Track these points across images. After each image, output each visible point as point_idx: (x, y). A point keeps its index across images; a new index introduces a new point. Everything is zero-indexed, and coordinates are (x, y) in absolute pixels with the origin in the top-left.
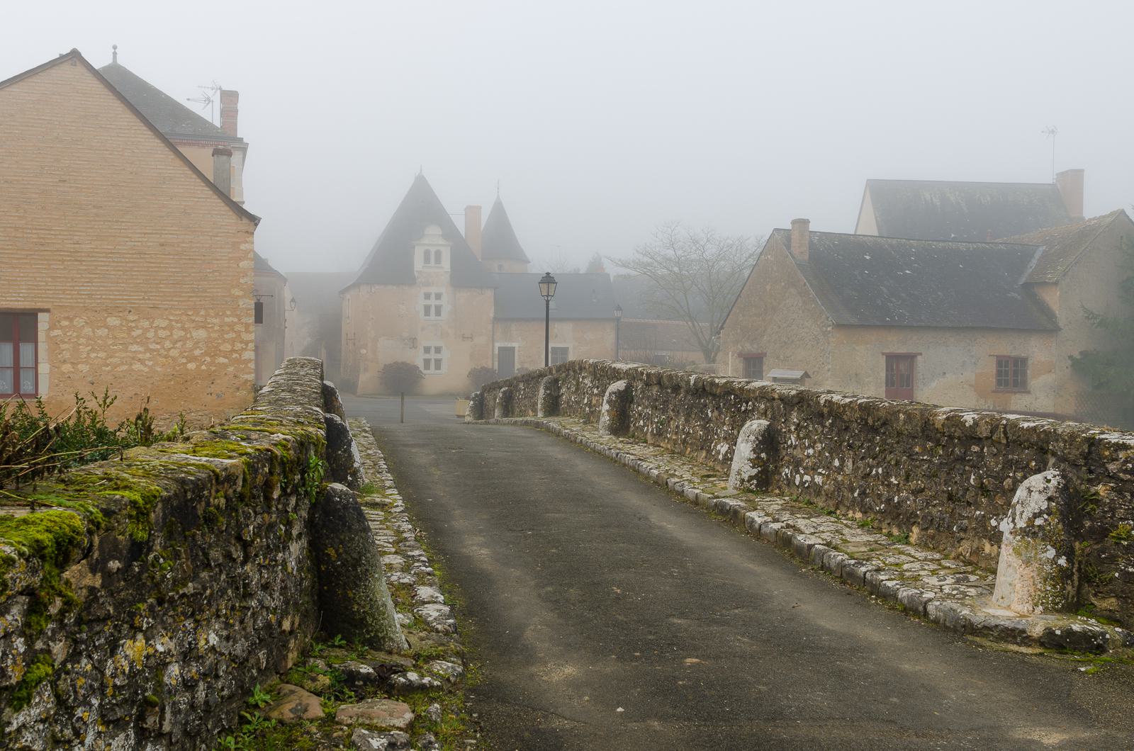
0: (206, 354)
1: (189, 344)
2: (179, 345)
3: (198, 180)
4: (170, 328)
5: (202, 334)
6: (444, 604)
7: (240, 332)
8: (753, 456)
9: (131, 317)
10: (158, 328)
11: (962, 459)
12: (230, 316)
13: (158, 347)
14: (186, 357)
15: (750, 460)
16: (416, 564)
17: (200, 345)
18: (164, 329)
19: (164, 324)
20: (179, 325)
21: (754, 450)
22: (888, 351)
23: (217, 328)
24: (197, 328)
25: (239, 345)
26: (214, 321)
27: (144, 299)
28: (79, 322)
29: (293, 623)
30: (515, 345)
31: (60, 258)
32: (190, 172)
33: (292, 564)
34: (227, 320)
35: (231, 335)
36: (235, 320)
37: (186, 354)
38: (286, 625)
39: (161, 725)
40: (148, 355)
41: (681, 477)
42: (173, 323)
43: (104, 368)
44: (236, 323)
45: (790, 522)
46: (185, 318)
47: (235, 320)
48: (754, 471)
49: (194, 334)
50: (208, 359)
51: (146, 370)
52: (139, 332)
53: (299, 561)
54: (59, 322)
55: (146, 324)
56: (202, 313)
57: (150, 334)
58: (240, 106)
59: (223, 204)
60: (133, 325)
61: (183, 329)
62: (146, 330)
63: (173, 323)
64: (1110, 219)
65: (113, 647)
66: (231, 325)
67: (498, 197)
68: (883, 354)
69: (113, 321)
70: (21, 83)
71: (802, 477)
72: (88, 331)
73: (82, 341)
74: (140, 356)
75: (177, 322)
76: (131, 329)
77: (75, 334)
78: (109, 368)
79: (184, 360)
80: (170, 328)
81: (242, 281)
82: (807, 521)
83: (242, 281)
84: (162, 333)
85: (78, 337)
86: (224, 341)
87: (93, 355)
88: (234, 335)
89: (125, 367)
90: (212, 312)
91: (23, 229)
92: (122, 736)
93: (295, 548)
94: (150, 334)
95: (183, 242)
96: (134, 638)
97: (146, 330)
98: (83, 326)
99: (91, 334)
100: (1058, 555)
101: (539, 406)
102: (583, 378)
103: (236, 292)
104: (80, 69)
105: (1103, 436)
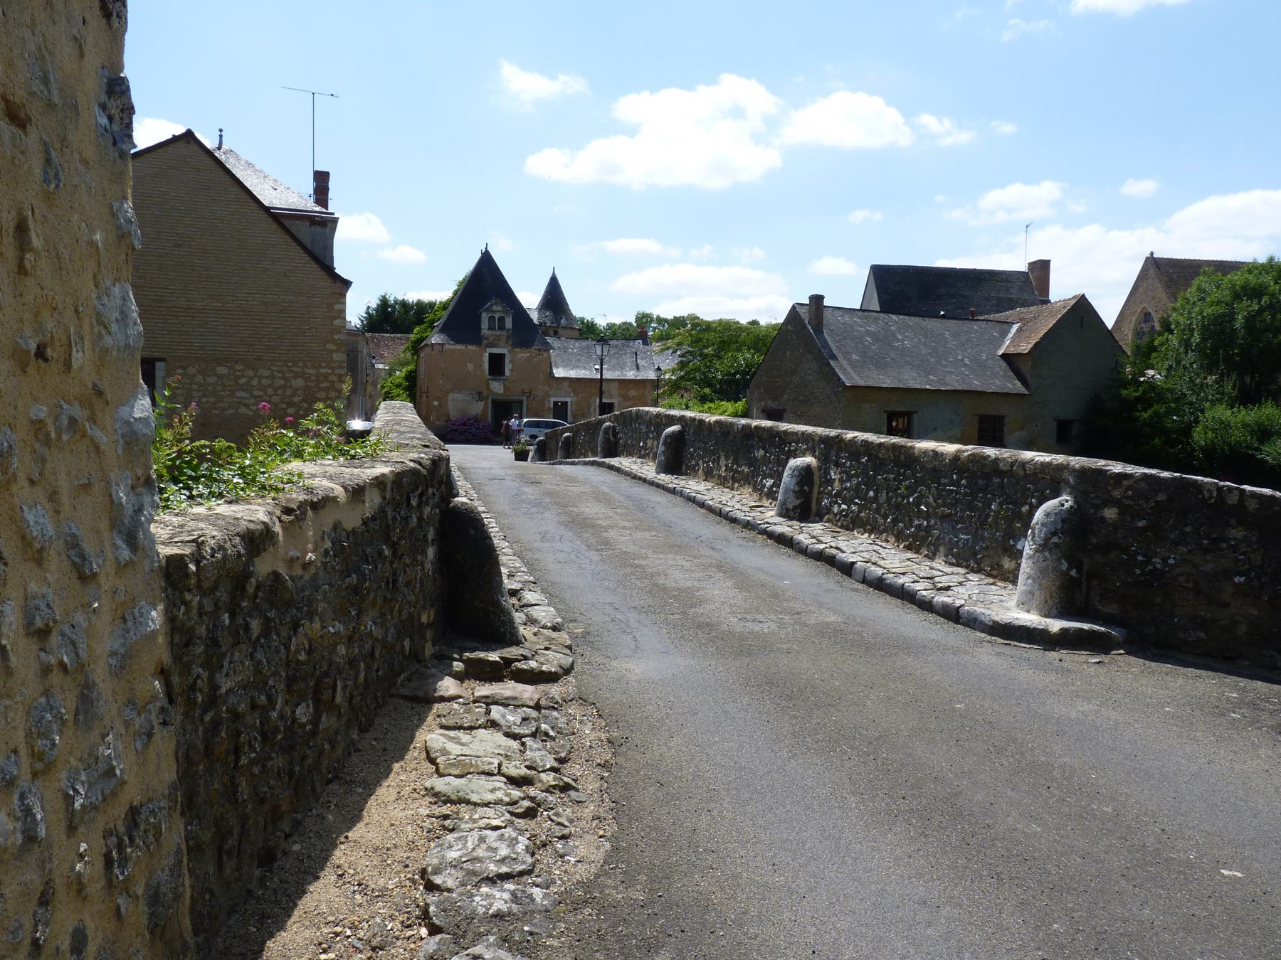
0: (304, 400)
1: (289, 392)
2: (280, 392)
3: (298, 248)
4: (272, 377)
5: (299, 383)
6: (549, 605)
7: (334, 381)
8: (797, 489)
9: (238, 367)
10: (261, 377)
11: (985, 490)
12: (325, 367)
13: (262, 393)
14: (286, 403)
15: (794, 491)
16: (519, 574)
17: (299, 392)
18: (267, 378)
19: (267, 373)
20: (280, 375)
21: (798, 483)
22: (888, 409)
23: (313, 378)
24: (296, 377)
25: (333, 393)
26: (311, 371)
27: (249, 351)
28: (191, 370)
29: (429, 617)
30: (568, 400)
31: (175, 314)
32: (291, 240)
33: (428, 566)
34: (322, 371)
35: (326, 385)
36: (330, 371)
37: (286, 400)
38: (424, 619)
39: (334, 697)
40: (252, 401)
41: (733, 507)
42: (275, 373)
43: (214, 412)
44: (330, 374)
45: (833, 544)
46: (284, 369)
47: (330, 371)
48: (797, 502)
49: (293, 383)
50: (305, 405)
51: (250, 413)
52: (245, 380)
53: (432, 563)
54: (174, 370)
55: (250, 373)
56: (301, 364)
57: (255, 382)
58: (331, 185)
59: (319, 269)
60: (239, 374)
61: (283, 378)
62: (251, 379)
63: (275, 373)
64: (1073, 302)
65: (295, 626)
66: (326, 376)
67: (554, 274)
68: (885, 411)
69: (222, 370)
70: (140, 158)
71: (840, 506)
72: (199, 378)
73: (195, 387)
74: (246, 401)
75: (279, 372)
76: (237, 377)
77: (188, 381)
78: (217, 412)
79: (284, 406)
80: (272, 377)
81: (336, 337)
82: (847, 543)
83: (336, 337)
84: (265, 382)
85: (191, 384)
86: (320, 389)
87: (204, 400)
88: (328, 385)
89: (232, 411)
90: (309, 364)
91: (143, 287)
92: (304, 704)
93: (431, 552)
94: (255, 382)
95: (284, 302)
96: (311, 620)
97: (251, 379)
98: (195, 374)
99: (202, 381)
100: (1070, 568)
101: (599, 449)
102: (640, 424)
103: (331, 346)
104: (194, 147)
105: (1108, 468)
